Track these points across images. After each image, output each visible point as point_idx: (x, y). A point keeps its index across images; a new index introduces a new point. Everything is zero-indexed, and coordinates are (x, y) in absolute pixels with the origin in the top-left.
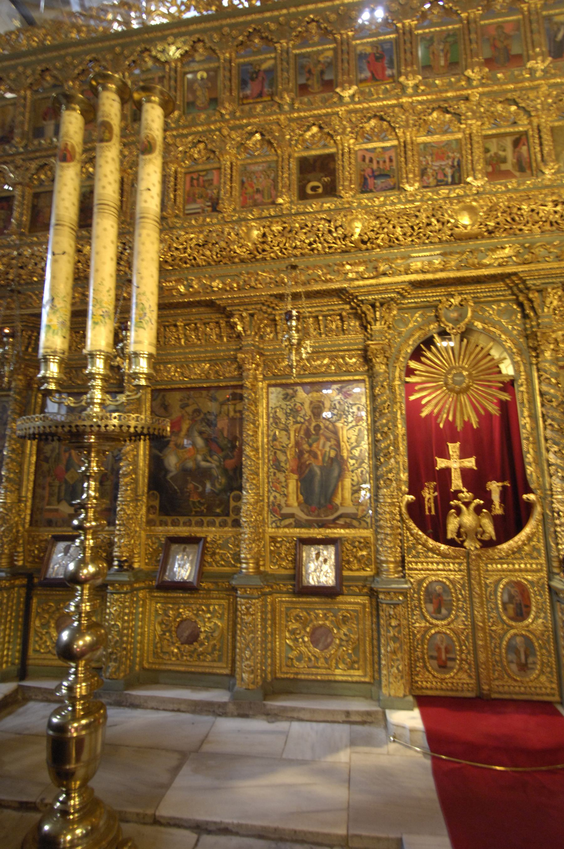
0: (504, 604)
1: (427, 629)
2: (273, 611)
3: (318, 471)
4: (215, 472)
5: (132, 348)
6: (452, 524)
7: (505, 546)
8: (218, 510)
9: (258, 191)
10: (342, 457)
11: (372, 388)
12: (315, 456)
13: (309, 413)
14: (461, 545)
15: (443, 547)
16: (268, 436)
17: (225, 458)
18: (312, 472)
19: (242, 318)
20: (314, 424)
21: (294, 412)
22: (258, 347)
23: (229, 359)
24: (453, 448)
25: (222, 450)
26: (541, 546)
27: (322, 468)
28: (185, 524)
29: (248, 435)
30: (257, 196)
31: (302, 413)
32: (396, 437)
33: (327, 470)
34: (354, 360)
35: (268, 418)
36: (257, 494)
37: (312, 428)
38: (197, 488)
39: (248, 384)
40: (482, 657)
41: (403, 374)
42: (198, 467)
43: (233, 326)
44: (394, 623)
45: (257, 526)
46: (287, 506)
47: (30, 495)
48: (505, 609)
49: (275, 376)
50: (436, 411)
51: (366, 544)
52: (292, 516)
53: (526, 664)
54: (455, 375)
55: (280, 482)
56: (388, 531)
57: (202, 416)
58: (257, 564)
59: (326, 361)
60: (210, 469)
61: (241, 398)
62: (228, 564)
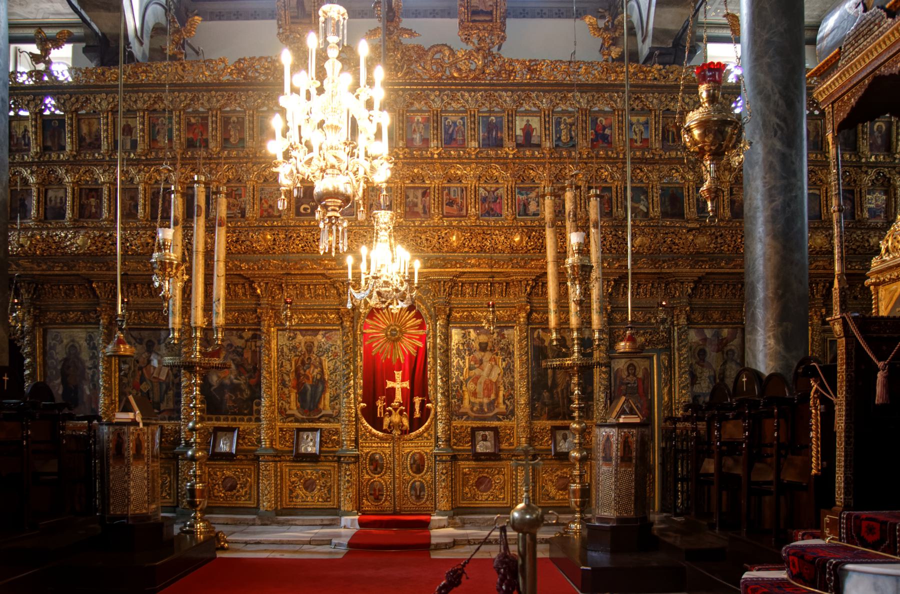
0: (411, 465)
1: (370, 480)
2: (282, 476)
3: (309, 387)
4: (243, 387)
6: (387, 421)
7: (413, 434)
8: (246, 412)
10: (324, 379)
12: (308, 378)
13: (304, 350)
15: (380, 434)
16: (278, 364)
17: (250, 377)
18: (305, 388)
20: (307, 357)
22: (271, 305)
23: (251, 310)
24: (398, 375)
25: (248, 372)
26: (433, 433)
27: (312, 386)
28: (224, 420)
29: (265, 363)
31: (300, 349)
34: (333, 316)
36: (271, 401)
37: (306, 359)
39: (265, 330)
40: (397, 492)
41: (362, 327)
42: (232, 383)
45: (271, 421)
46: (290, 409)
47: (117, 399)
48: (411, 468)
50: (380, 351)
52: (293, 415)
53: (420, 495)
54: (392, 330)
55: (285, 394)
57: (233, 348)
59: (316, 315)
60: (240, 384)
62: (253, 445)
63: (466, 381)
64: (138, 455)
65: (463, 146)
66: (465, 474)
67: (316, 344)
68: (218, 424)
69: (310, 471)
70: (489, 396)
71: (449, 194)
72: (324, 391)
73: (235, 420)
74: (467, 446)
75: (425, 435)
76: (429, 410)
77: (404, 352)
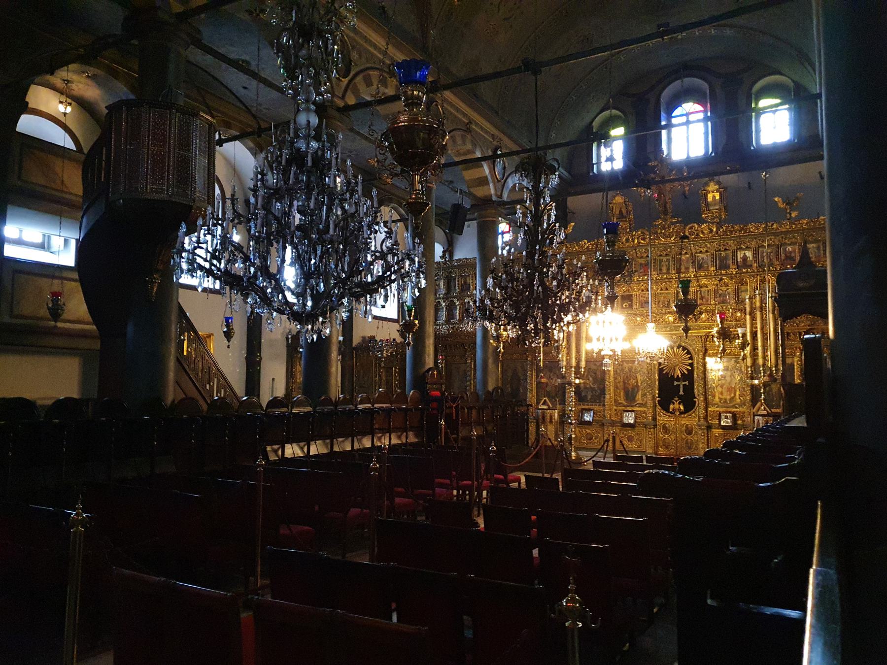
3: (630, 389)
14: (674, 413)
21: (623, 370)
27: (632, 388)
33: (633, 389)
42: (591, 387)
52: (621, 403)
58: (610, 417)
62: (601, 417)
63: (717, 387)
64: (551, 422)
65: (707, 269)
66: (716, 436)
67: (634, 368)
68: (584, 407)
69: (631, 433)
70: (730, 395)
71: (701, 294)
72: (638, 391)
74: (717, 422)
75: (693, 415)
77: (681, 372)
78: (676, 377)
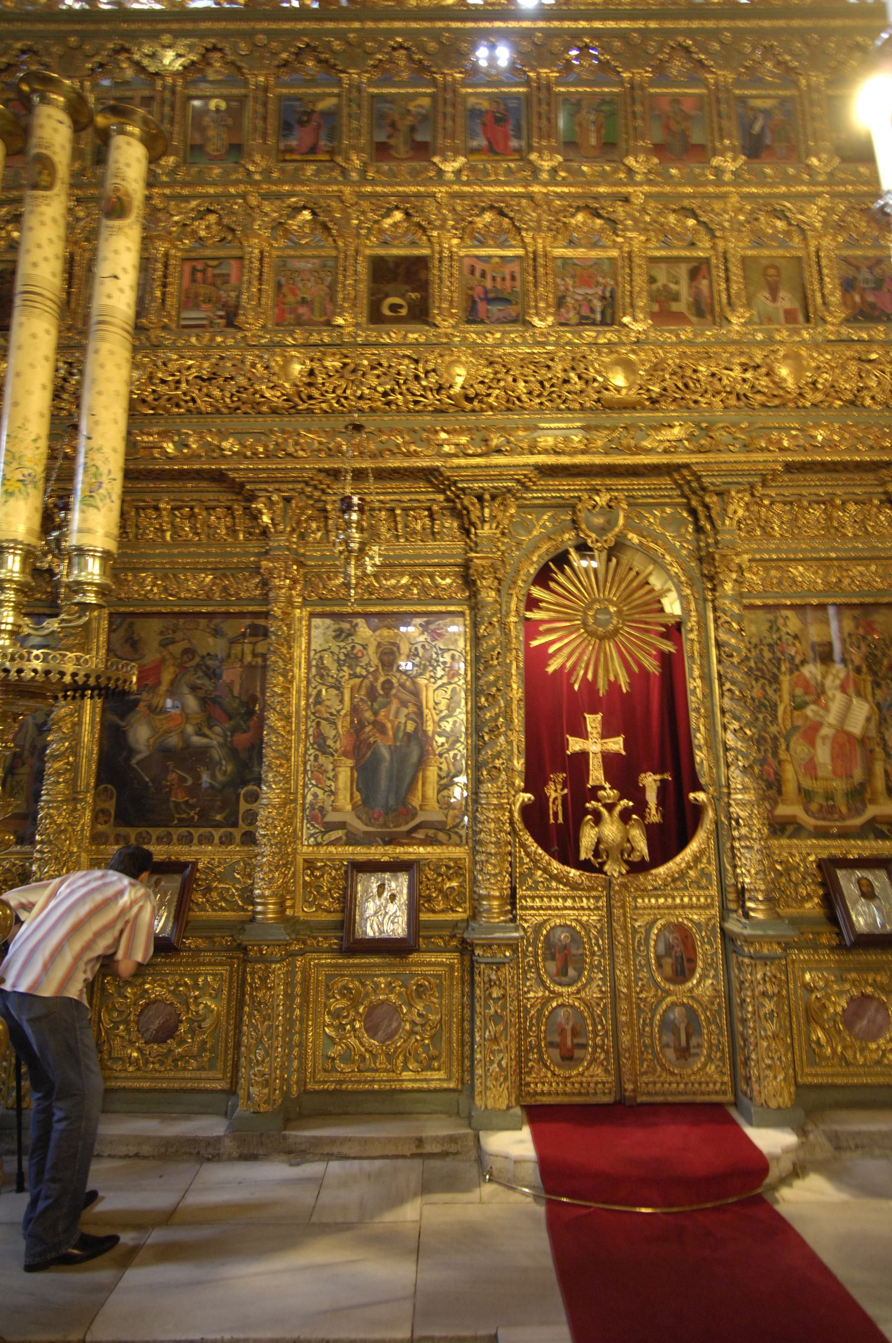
0: (658, 958)
2: (305, 980)
5: (74, 540)
6: (588, 837)
9: (304, 301)
11: (475, 625)
12: (382, 730)
14: (600, 870)
16: (308, 696)
19: (270, 504)
24: (593, 722)
26: (712, 869)
30: (302, 310)
32: (508, 703)
35: (309, 667)
38: (183, 780)
42: (188, 745)
43: (255, 516)
44: (496, 993)
49: (322, 600)
51: (456, 869)
52: (342, 825)
56: (492, 849)
61: (265, 633)
62: (233, 906)
73: (188, 840)
76: (698, 810)
78: (602, 688)
